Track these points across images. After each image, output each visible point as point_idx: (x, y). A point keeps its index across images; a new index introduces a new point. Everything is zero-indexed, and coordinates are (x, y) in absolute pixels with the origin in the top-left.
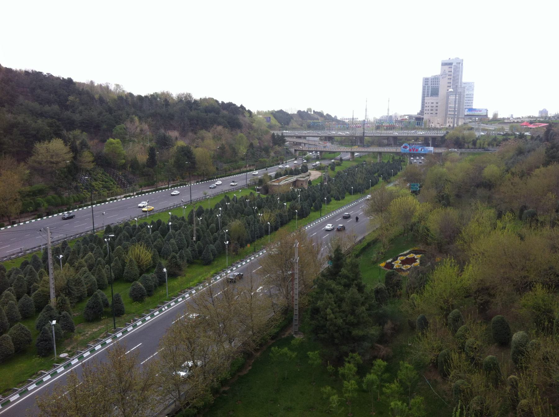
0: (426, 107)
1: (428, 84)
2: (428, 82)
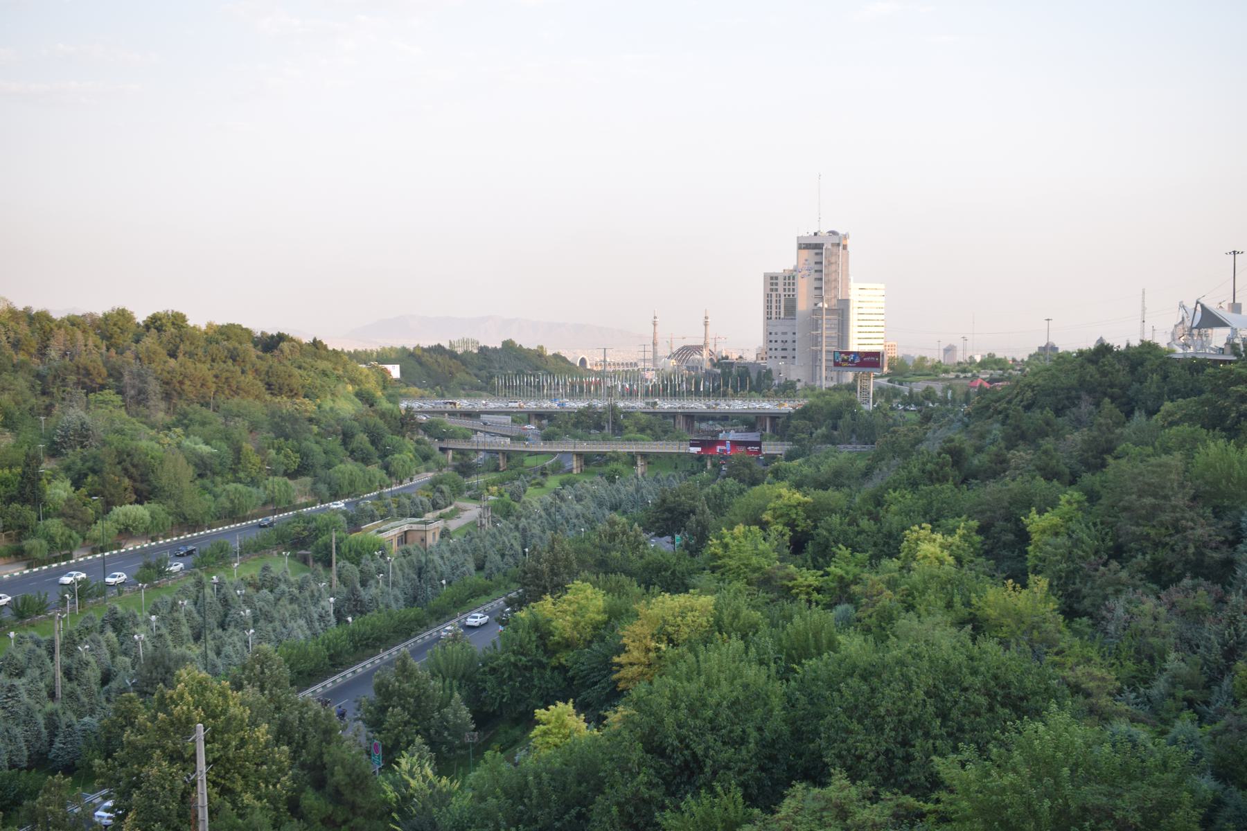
1: (777, 290)
2: (777, 284)
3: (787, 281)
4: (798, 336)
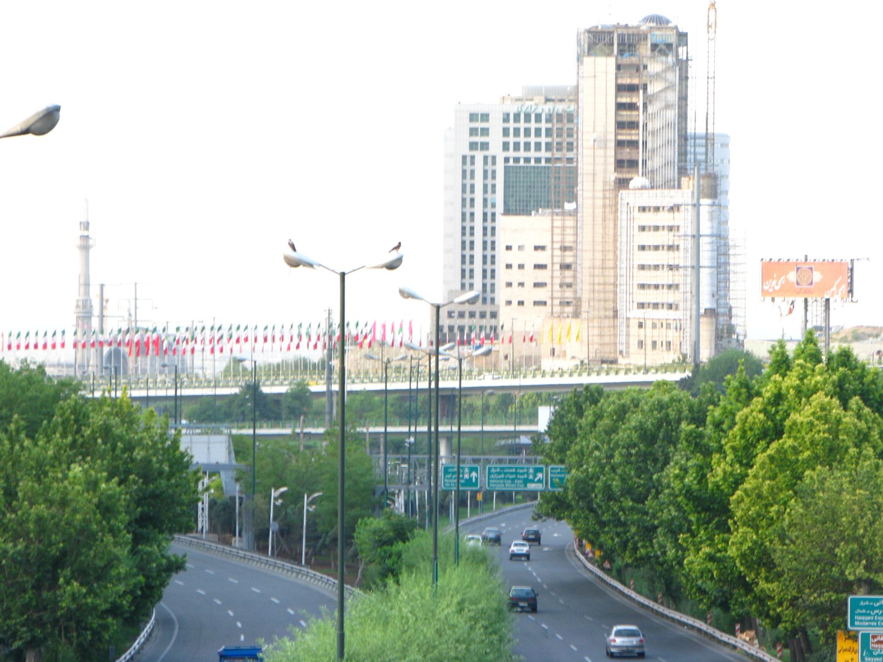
0: (509, 266)
1: (485, 146)
2: (485, 132)
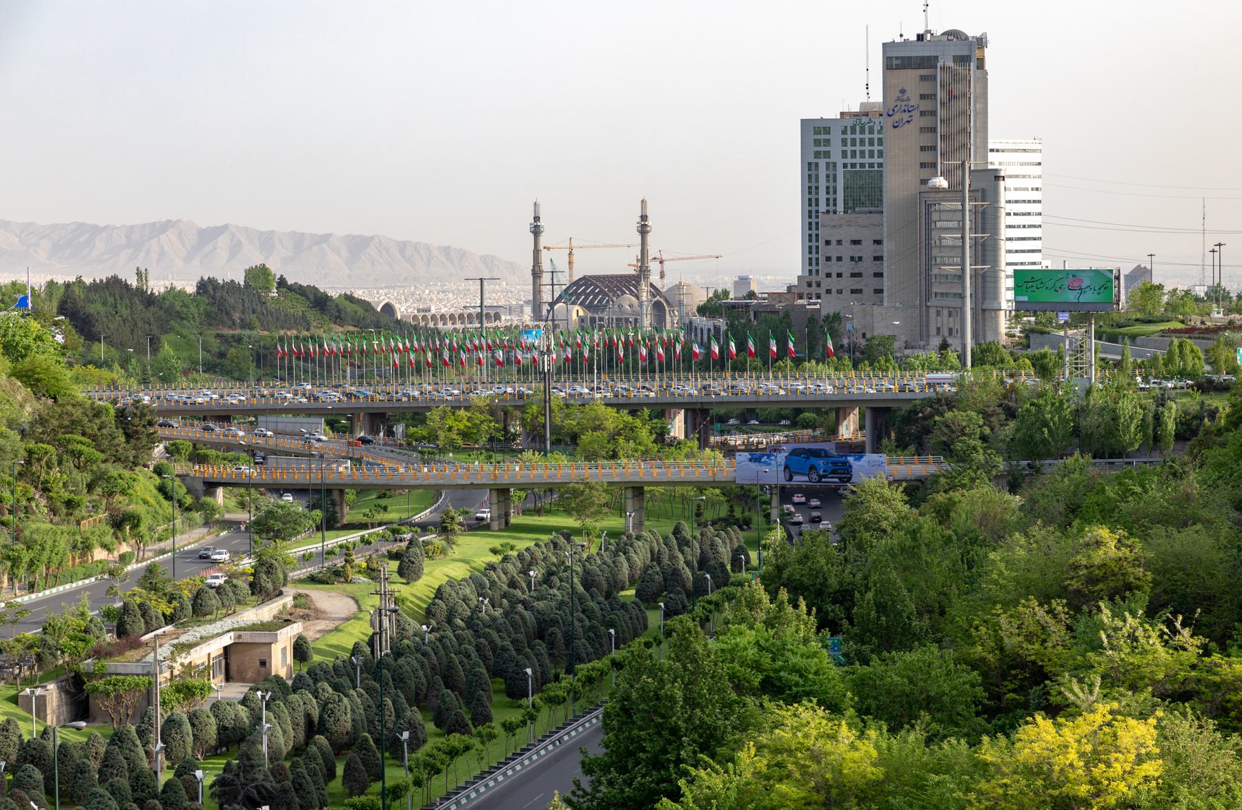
1: (827, 154)
2: (827, 142)
3: (849, 136)
4: (887, 248)
